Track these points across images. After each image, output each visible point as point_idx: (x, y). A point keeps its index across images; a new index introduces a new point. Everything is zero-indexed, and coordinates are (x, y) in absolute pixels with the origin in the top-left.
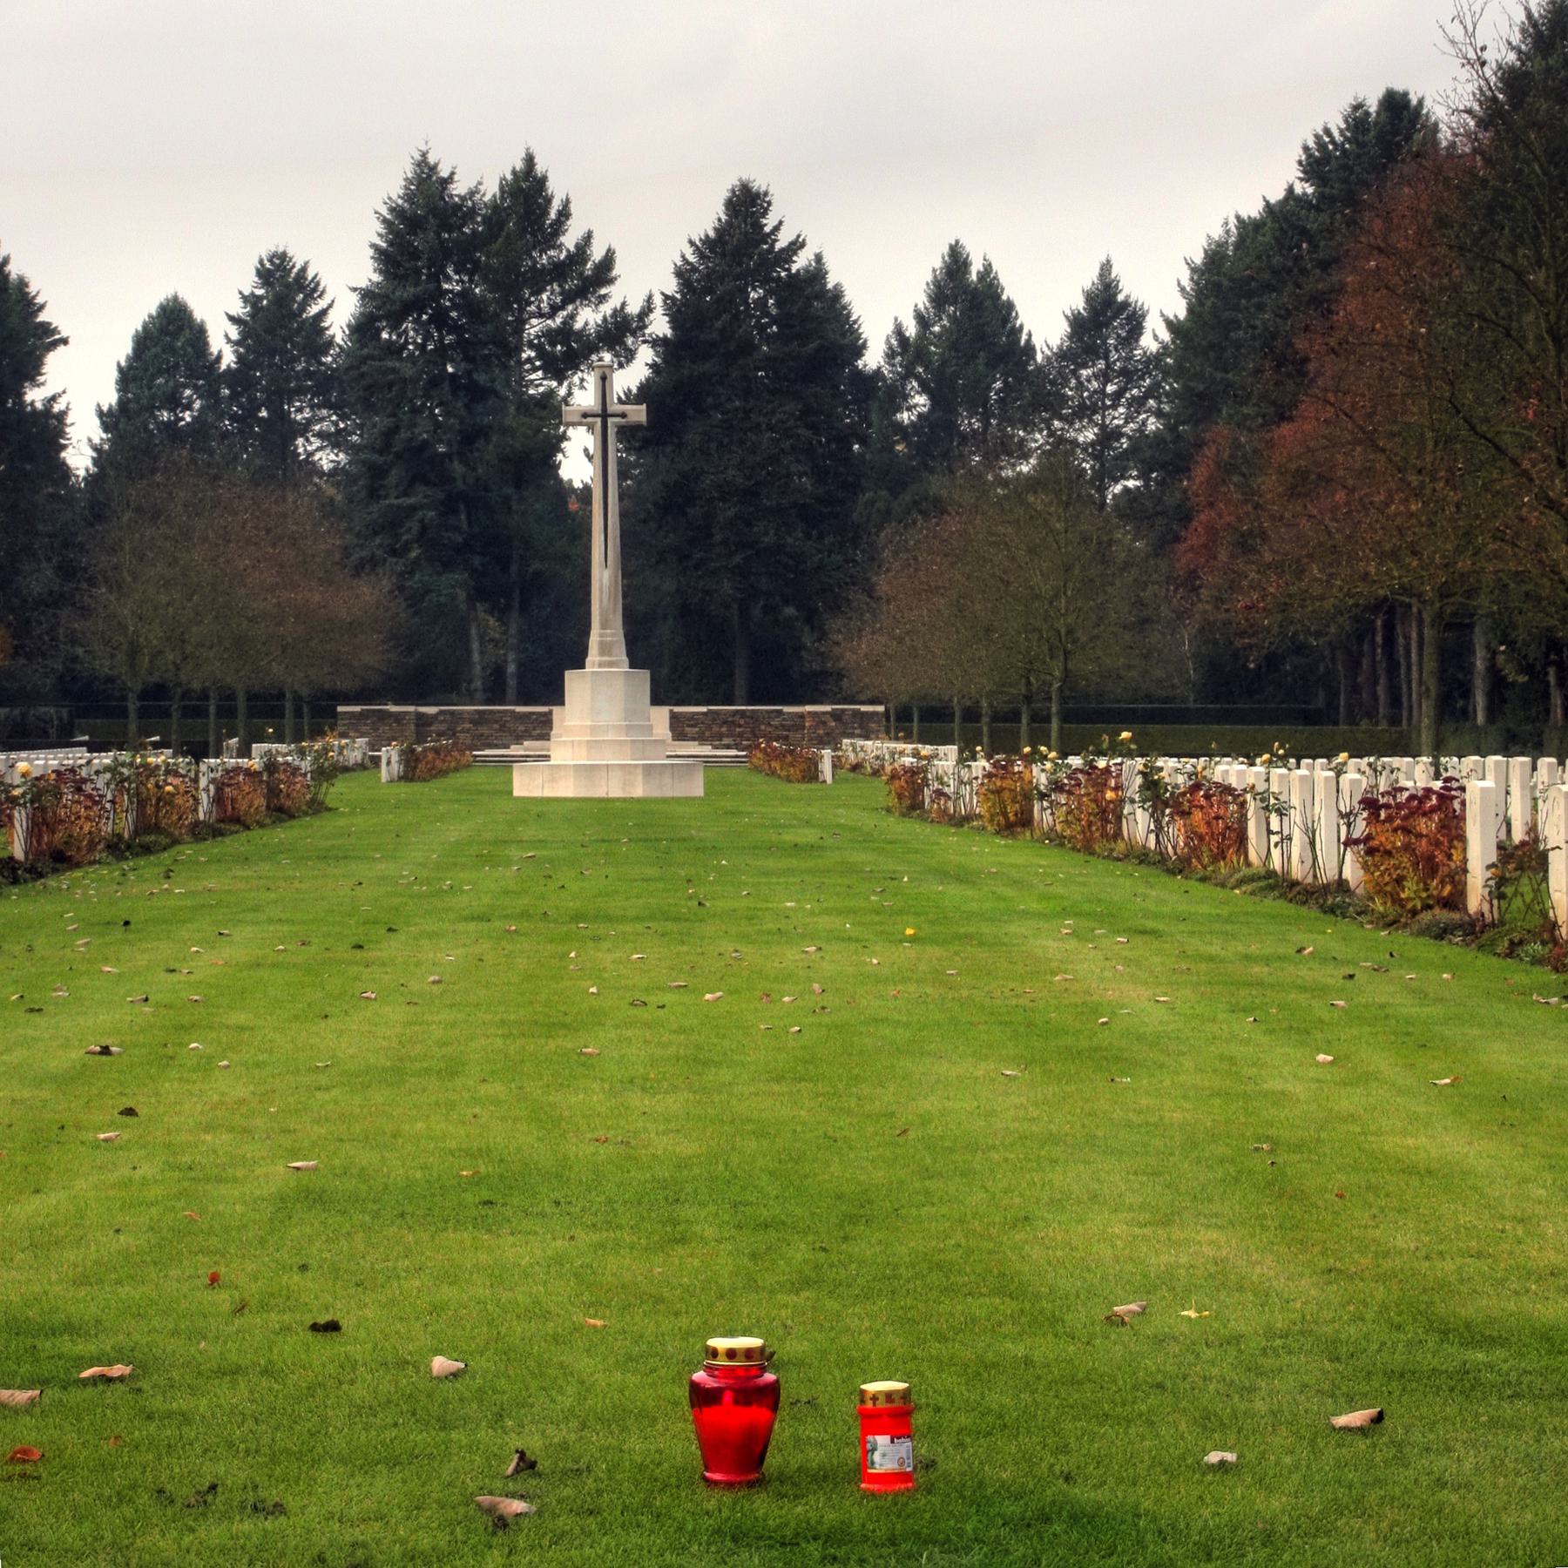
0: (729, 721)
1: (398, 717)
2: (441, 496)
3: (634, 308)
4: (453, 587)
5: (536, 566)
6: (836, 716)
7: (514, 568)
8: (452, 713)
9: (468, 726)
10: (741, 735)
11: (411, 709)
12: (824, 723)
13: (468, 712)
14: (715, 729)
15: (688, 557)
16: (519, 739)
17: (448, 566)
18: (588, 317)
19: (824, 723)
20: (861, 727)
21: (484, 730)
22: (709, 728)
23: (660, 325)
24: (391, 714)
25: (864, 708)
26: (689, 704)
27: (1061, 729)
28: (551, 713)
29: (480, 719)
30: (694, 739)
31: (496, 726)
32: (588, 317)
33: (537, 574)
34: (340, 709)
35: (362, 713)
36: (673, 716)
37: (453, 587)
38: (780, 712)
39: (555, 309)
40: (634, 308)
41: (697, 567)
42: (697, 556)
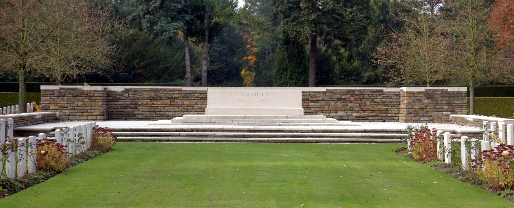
0: (342, 99)
1: (89, 95)
4: (176, 29)
5: (215, 20)
6: (428, 95)
7: (206, 21)
8: (135, 91)
9: (146, 101)
10: (352, 109)
11: (100, 88)
12: (419, 100)
13: (146, 91)
14: (332, 104)
15: (289, 16)
17: (174, 19)
19: (419, 100)
20: (448, 103)
21: (158, 104)
22: (328, 103)
24: (83, 92)
25: (450, 89)
26: (189, 92)
27: (474, 99)
28: (206, 93)
30: (322, 112)
31: (168, 101)
33: (217, 24)
34: (42, 87)
35: (60, 91)
36: (304, 94)
37: (176, 29)
38: (382, 92)
41: (293, 21)
42: (293, 15)
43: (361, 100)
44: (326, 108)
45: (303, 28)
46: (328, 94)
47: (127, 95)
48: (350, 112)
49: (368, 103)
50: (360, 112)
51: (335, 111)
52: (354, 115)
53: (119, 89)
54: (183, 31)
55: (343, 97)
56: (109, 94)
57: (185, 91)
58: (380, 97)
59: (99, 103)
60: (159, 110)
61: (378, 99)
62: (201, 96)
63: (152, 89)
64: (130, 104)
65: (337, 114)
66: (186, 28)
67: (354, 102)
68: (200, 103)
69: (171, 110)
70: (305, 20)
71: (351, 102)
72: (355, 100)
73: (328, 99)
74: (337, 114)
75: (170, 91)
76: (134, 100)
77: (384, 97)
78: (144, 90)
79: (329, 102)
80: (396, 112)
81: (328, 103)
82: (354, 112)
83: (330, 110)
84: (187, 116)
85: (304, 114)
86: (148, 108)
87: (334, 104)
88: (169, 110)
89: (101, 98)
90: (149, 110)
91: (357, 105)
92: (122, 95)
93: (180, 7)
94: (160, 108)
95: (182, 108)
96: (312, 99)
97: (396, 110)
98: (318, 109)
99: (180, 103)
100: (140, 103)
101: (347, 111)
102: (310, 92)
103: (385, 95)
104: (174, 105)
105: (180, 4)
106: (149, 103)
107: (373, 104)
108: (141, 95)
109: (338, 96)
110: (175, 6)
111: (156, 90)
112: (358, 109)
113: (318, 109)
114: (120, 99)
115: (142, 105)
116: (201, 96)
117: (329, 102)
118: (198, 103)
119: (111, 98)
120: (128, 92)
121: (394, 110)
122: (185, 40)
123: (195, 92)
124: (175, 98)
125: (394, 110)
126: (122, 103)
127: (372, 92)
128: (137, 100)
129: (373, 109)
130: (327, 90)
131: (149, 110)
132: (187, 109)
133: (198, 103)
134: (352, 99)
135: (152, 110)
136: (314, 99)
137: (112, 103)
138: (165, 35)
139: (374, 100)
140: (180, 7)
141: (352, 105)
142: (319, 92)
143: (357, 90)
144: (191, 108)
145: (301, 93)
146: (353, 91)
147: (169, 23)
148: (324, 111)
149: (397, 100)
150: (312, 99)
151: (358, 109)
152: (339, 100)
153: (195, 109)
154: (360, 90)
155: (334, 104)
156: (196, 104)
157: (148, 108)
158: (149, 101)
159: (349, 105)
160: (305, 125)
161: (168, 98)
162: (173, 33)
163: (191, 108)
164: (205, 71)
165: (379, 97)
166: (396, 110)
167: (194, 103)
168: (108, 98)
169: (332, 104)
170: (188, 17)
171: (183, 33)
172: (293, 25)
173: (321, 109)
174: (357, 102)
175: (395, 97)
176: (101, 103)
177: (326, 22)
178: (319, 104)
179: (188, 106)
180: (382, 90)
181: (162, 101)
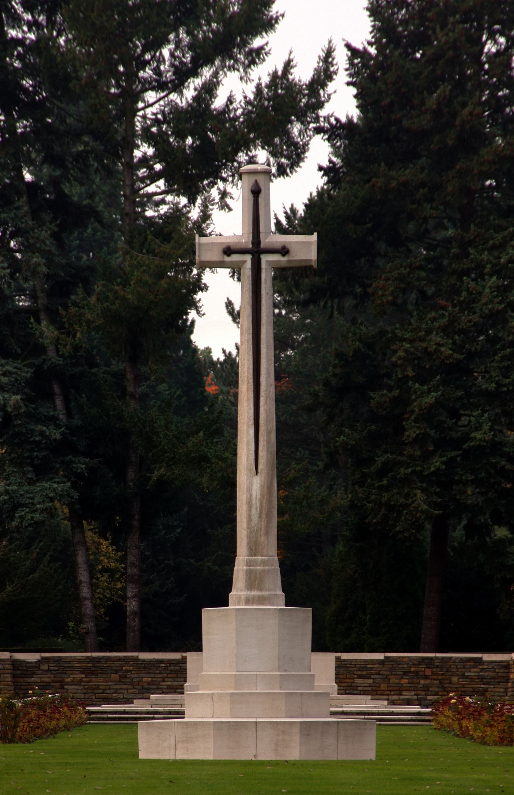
0: (413, 672)
2: (28, 373)
3: (303, 74)
4: (52, 500)
10: (426, 689)
14: (394, 680)
16: (144, 692)
17: (43, 471)
18: (235, 88)
21: (99, 681)
22: (386, 679)
23: (342, 103)
26: (151, 660)
29: (93, 669)
31: (115, 677)
32: (235, 88)
36: (340, 665)
37: (52, 500)
39: (183, 74)
40: (303, 74)
42: (380, 460)
43: (443, 674)
44: (383, 687)
45: (408, 494)
46: (388, 665)
47: (46, 667)
48: (423, 693)
49: (455, 679)
50: (440, 693)
51: (397, 692)
52: (429, 697)
53: (32, 657)
54: (71, 506)
55: (413, 669)
56: (16, 664)
57: (143, 660)
58: (477, 670)
59: (7, 679)
60: (100, 691)
61: (473, 673)
62: (172, 668)
63: (88, 657)
64: (53, 681)
65: (402, 697)
66: (76, 495)
67: (431, 677)
68: (170, 679)
69: (121, 691)
70: (414, 472)
71: (426, 677)
72: (433, 674)
73: (387, 673)
74: (402, 697)
75: (119, 659)
76: (59, 676)
77: (483, 669)
78: (74, 658)
79: (389, 677)
80: (502, 694)
81: (386, 679)
82: (430, 693)
83: (390, 691)
84: (153, 697)
85: (338, 694)
86: (82, 687)
87: (397, 681)
88: (118, 691)
89: (9, 671)
90: (85, 691)
91: (435, 682)
92: (38, 667)
93: (58, 436)
94: (103, 687)
95: (140, 687)
96: (359, 673)
97: (502, 690)
98: (369, 689)
99: (137, 680)
100: (69, 680)
101: (419, 692)
102: (356, 661)
103: (485, 667)
104: (125, 683)
105: (58, 427)
106: (84, 679)
107: (463, 681)
108: (69, 667)
109: (404, 668)
110: (42, 434)
111: (93, 659)
112: (437, 689)
113: (369, 689)
114: (34, 673)
115: (72, 683)
116: (172, 668)
117: (389, 677)
118: (166, 680)
119: (19, 672)
120: (48, 662)
121: (498, 690)
122: (73, 528)
123: (161, 661)
124: (127, 671)
125: (498, 690)
126: (38, 680)
127: (462, 660)
128: (64, 676)
129: (463, 689)
130: (386, 658)
131: (85, 691)
132: (148, 689)
133: (166, 680)
134: (428, 672)
135: (90, 691)
136: (364, 673)
137: (22, 680)
138: (21, 517)
139: (466, 674)
140: (58, 436)
141: (428, 681)
142: (372, 662)
143: (437, 658)
144: (155, 687)
145: (334, 660)
146: (431, 659)
147: (31, 482)
148: (379, 692)
149: (504, 675)
150: (359, 673)
151: (437, 689)
152: (405, 674)
153: (162, 689)
154: (443, 658)
155: (397, 681)
156: (163, 681)
157: (82, 687)
158: (83, 676)
159: (422, 682)
160: (337, 707)
161: (116, 672)
162: (43, 511)
163: (155, 687)
164: (134, 613)
165: (474, 670)
166: (502, 690)
167: (159, 680)
168: (15, 672)
169: (394, 680)
170: (81, 465)
171: (66, 510)
172: (380, 487)
173: (374, 688)
174: (436, 677)
175: (502, 670)
176: (10, 679)
177: (471, 477)
178: (370, 681)
179: (149, 683)
180: (480, 659)
181: (105, 676)
